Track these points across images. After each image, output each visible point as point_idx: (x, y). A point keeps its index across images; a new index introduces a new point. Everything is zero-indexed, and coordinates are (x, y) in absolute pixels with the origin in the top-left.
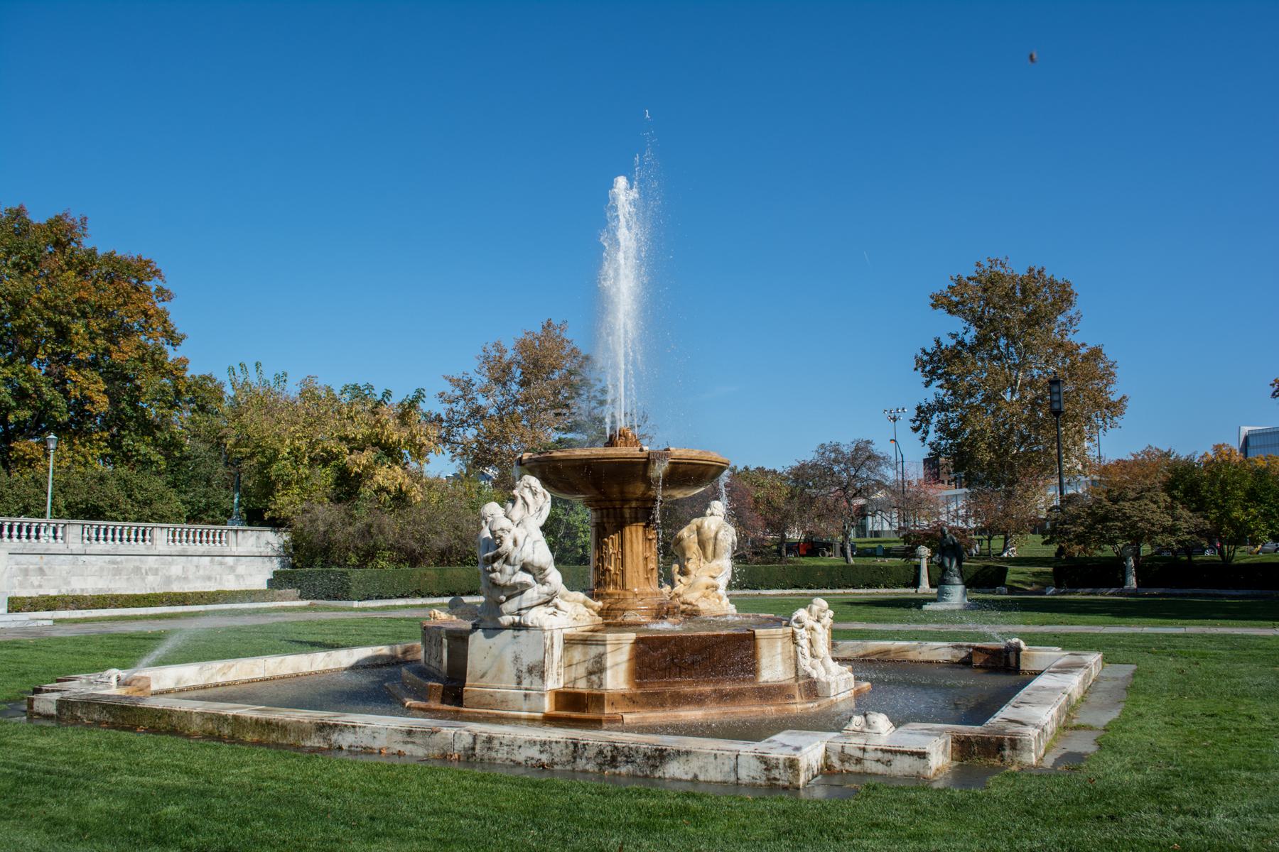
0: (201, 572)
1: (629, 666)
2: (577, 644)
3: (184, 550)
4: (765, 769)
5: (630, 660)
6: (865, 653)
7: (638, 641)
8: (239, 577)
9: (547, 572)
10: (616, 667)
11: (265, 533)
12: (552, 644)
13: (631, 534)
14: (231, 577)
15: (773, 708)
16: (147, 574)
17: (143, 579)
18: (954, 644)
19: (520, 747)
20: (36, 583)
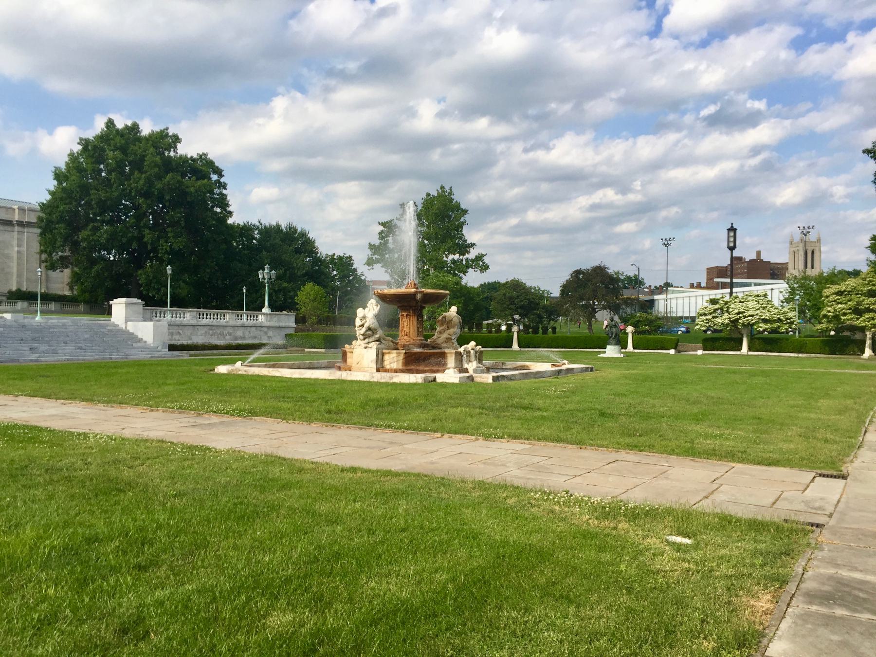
7: (406, 353)
8: (269, 337)
14: (266, 337)
17: (225, 337)
20: (177, 339)
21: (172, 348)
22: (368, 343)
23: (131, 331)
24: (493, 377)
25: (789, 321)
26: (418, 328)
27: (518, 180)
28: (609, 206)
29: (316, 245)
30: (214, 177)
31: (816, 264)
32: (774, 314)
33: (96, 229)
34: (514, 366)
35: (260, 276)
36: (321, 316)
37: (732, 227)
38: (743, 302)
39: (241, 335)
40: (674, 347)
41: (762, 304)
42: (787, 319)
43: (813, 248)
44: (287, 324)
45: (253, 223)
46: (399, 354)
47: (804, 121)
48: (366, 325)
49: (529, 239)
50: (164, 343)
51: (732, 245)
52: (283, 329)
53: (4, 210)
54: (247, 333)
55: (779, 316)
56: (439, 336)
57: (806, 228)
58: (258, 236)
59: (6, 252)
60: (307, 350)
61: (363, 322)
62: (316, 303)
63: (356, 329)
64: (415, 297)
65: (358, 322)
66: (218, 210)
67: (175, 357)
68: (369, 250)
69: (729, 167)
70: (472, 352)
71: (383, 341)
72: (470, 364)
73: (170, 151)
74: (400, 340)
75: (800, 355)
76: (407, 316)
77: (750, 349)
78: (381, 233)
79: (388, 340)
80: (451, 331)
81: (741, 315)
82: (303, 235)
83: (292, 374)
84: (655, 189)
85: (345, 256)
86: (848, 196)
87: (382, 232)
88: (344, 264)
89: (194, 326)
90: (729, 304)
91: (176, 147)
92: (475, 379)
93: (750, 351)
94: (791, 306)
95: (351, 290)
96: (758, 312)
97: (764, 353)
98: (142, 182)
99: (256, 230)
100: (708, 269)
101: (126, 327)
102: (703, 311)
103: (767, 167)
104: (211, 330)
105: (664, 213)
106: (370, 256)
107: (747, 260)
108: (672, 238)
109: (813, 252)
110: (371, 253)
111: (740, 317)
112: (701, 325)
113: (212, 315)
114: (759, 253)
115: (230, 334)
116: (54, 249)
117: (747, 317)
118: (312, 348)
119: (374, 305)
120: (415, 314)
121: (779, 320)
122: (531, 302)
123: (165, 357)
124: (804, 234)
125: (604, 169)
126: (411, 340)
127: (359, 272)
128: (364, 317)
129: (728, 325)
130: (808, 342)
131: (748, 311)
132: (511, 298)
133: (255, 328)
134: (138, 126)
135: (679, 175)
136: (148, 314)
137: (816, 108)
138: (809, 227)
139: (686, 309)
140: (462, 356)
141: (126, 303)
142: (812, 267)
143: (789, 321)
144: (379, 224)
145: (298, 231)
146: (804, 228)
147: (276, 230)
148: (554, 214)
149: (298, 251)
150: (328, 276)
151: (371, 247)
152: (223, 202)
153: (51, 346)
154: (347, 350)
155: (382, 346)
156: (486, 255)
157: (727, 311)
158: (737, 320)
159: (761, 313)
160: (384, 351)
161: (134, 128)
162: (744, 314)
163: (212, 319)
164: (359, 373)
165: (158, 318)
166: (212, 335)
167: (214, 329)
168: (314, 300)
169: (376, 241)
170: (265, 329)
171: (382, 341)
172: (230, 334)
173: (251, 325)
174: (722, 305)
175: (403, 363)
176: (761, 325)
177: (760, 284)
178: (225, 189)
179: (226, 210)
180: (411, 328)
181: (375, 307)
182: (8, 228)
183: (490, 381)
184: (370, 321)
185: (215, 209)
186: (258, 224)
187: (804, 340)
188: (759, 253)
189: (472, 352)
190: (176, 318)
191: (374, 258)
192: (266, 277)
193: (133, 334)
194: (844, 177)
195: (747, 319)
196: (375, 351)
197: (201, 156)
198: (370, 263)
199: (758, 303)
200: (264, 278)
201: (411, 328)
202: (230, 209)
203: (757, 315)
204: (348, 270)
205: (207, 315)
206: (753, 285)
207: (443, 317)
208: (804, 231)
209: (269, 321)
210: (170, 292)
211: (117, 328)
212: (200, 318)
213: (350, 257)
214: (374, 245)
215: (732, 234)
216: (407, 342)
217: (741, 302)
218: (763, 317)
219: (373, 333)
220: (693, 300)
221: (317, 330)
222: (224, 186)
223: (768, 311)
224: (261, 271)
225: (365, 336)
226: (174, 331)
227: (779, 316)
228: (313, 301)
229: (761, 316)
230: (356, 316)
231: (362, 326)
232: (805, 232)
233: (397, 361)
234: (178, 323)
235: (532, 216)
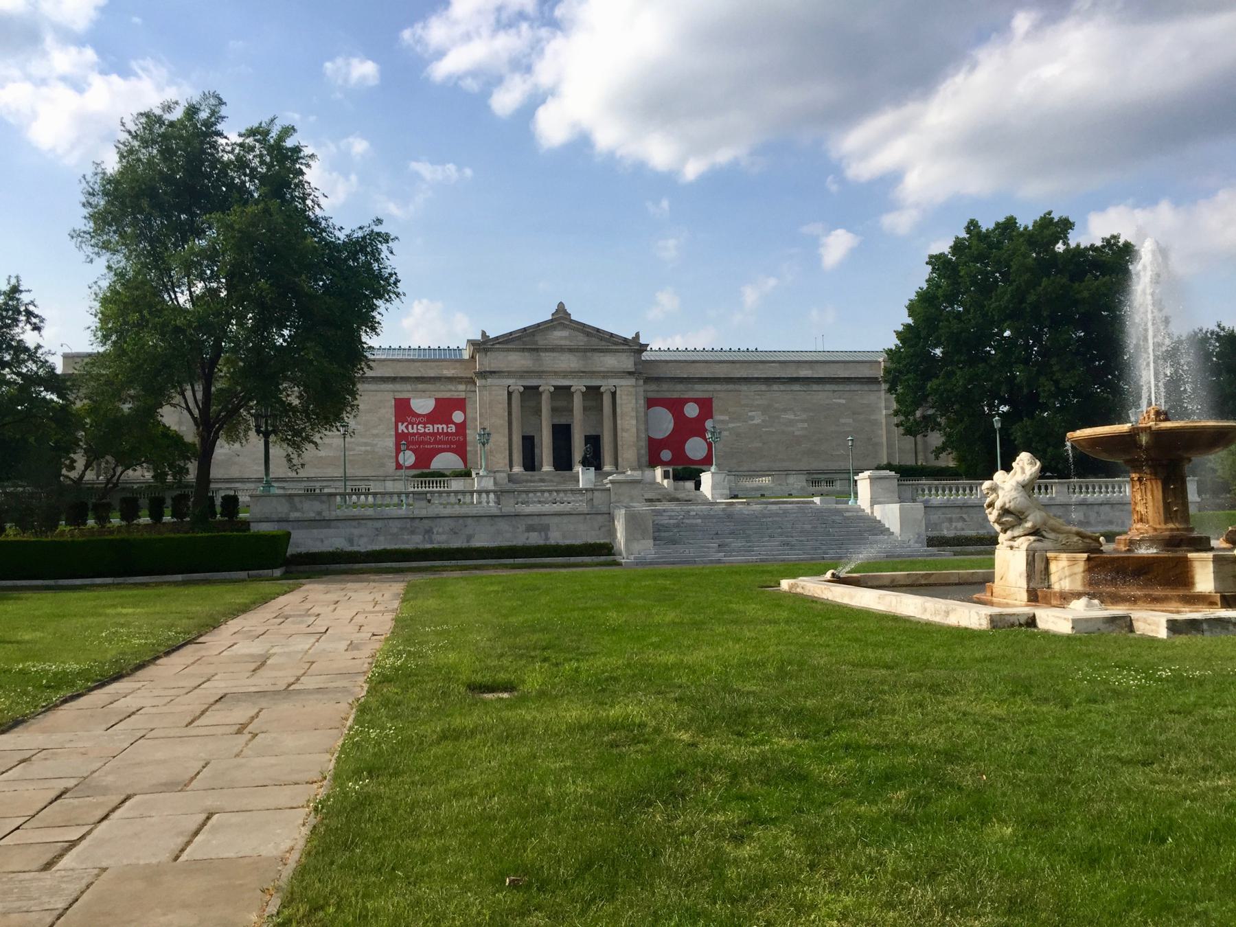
0: (1103, 517)
3: (1085, 500)
5: (1084, 572)
7: (1089, 559)
9: (1026, 514)
21: (933, 542)
22: (1013, 539)
23: (878, 518)
24: (1169, 621)
33: (950, 375)
39: (1082, 518)
46: (1073, 562)
48: (998, 504)
52: (496, 519)
53: (868, 365)
59: (873, 417)
67: (927, 556)
79: (1069, 532)
91: (1066, 237)
92: (1136, 624)
101: (872, 513)
116: (917, 404)
136: (908, 493)
139: (392, 461)
141: (870, 477)
153: (749, 542)
160: (1049, 555)
173: (1100, 501)
182: (874, 387)
183: (1162, 633)
186: (1217, 329)
190: (1101, 492)
193: (880, 521)
197: (1108, 241)
201: (1150, 504)
210: (1001, 453)
211: (860, 514)
233: (1070, 575)
234: (959, 503)
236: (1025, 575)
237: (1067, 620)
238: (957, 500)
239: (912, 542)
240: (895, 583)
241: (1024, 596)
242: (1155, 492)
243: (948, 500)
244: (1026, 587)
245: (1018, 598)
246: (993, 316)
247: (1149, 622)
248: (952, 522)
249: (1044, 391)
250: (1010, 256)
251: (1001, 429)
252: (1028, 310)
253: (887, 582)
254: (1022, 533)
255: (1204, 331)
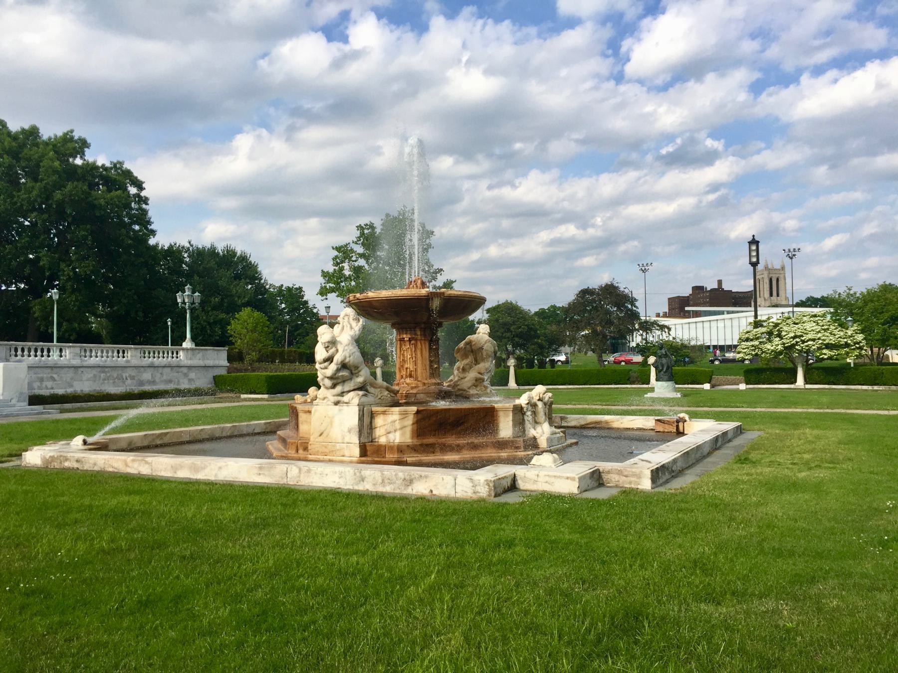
0: (165, 377)
1: (413, 428)
2: (380, 414)
3: (152, 363)
4: (473, 486)
5: (413, 424)
6: (585, 423)
7: (418, 412)
8: (190, 380)
9: (360, 369)
10: (404, 429)
11: (209, 352)
12: (363, 414)
13: (422, 346)
14: (186, 381)
15: (505, 454)
16: (126, 379)
17: (124, 382)
18: (657, 418)
19: (327, 475)
20: (49, 387)
21: (35, 400)
22: (342, 394)
25: (858, 346)
26: (431, 362)
27: (478, 215)
28: (572, 240)
29: (259, 269)
30: (133, 190)
31: (781, 293)
32: (839, 337)
34: (583, 423)
35: (179, 300)
36: (263, 351)
37: (754, 239)
38: (797, 324)
39: (150, 378)
40: (709, 381)
41: (823, 326)
42: (855, 343)
43: (777, 275)
44: (217, 363)
45: (182, 244)
46: (404, 415)
47: (757, 159)
48: (338, 358)
49: (490, 273)
50: (21, 394)
51: (754, 260)
52: (209, 368)
54: (158, 375)
55: (845, 340)
56: (462, 376)
57: (792, 250)
58: (188, 260)
60: (243, 396)
61: (332, 351)
62: (256, 335)
63: (317, 366)
64: (428, 304)
65: (320, 353)
66: (137, 228)
68: (322, 278)
69: (687, 203)
70: (540, 404)
71: (371, 390)
72: (539, 429)
73: (75, 157)
74: (398, 384)
75: (876, 388)
76: (410, 340)
77: (807, 381)
78: (335, 258)
80: (482, 366)
81: (798, 340)
82: (244, 258)
83: (175, 469)
84: (615, 224)
85: (295, 287)
86: (800, 230)
87: (336, 257)
88: (294, 296)
89: (76, 368)
90: (780, 326)
92: (605, 477)
93: (807, 384)
94: (856, 328)
95: (302, 325)
96: (819, 335)
97: (827, 386)
98: (35, 193)
99: (186, 252)
100: (669, 299)
102: (747, 336)
103: (722, 202)
104: (103, 372)
105: (622, 248)
106: (323, 285)
107: (708, 289)
108: (649, 264)
109: (778, 280)
110: (324, 281)
111: (797, 342)
112: (745, 353)
113: (105, 351)
114: (720, 282)
115: (133, 378)
117: (807, 342)
118: (251, 393)
119: (351, 317)
120: (425, 336)
121: (847, 345)
122: (530, 329)
123: (18, 415)
124: (790, 257)
125: (566, 204)
126: (420, 384)
127: (310, 304)
128: (333, 343)
129: (781, 353)
130: (884, 371)
131: (807, 334)
132: (505, 324)
133: (170, 369)
134: (38, 129)
135: (635, 210)
137: (769, 146)
138: (794, 250)
140: (524, 414)
142: (778, 295)
143: (858, 346)
144: (333, 248)
145: (238, 254)
146: (789, 251)
147: (212, 253)
148: (515, 249)
149: (237, 277)
150: (274, 307)
151: (325, 274)
152: (143, 219)
154: (300, 407)
155: (370, 399)
156: (455, 281)
157: (779, 336)
158: (793, 346)
159: (823, 336)
160: (374, 409)
161: (33, 132)
162: (803, 339)
163: (105, 358)
164: (328, 469)
165: (19, 357)
166: (104, 380)
167: (109, 372)
168: (254, 330)
169: (330, 268)
170: (185, 370)
171: (368, 388)
172: (133, 378)
174: (771, 328)
175: (413, 431)
176: (825, 351)
177: (733, 312)
178: (147, 204)
179: (147, 228)
180: (419, 362)
181: (354, 324)
183: (646, 484)
184: (346, 351)
185: (133, 227)
187: (879, 369)
188: (720, 282)
189: (540, 404)
191: (328, 287)
192: (186, 300)
194: (795, 212)
195: (806, 344)
196: (357, 409)
197: (115, 165)
198: (323, 292)
199: (818, 324)
200: (184, 303)
201: (419, 362)
202: (152, 227)
203: (819, 339)
204: (297, 302)
205: (149, 353)
206: (725, 312)
207: (467, 344)
208: (790, 254)
209: (191, 359)
212: (145, 357)
213: (300, 288)
214: (328, 272)
215: (754, 247)
216: (412, 388)
217: (795, 323)
218: (827, 342)
219: (352, 373)
220: (735, 322)
221: (258, 369)
222: (146, 201)
223: (831, 333)
224: (180, 293)
225: (336, 380)
226: (45, 376)
227: (845, 340)
228: (252, 331)
229: (824, 340)
230: (318, 342)
231: (330, 359)
232: (791, 256)
233: (401, 429)
235: (493, 251)
236: (358, 430)
237: (573, 479)
238: (49, 361)
239: (14, 402)
240: (133, 446)
241: (356, 451)
242: (424, 350)
243: (40, 361)
244: (358, 442)
245: (347, 454)
246: (22, 205)
247: (626, 473)
248: (43, 381)
249: (64, 275)
250: (40, 157)
251: (58, 301)
252: (54, 206)
253: (124, 445)
254: (352, 388)
255: (177, 246)
